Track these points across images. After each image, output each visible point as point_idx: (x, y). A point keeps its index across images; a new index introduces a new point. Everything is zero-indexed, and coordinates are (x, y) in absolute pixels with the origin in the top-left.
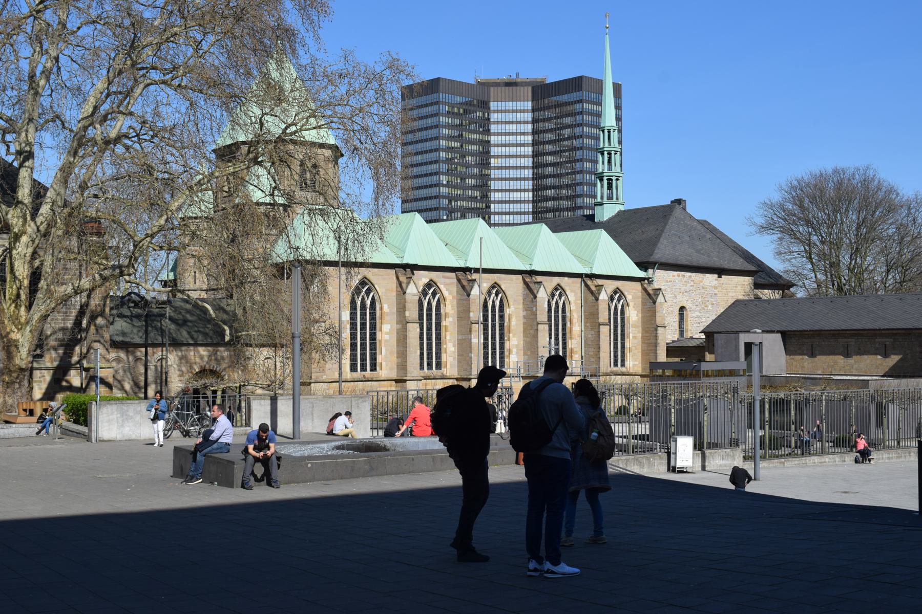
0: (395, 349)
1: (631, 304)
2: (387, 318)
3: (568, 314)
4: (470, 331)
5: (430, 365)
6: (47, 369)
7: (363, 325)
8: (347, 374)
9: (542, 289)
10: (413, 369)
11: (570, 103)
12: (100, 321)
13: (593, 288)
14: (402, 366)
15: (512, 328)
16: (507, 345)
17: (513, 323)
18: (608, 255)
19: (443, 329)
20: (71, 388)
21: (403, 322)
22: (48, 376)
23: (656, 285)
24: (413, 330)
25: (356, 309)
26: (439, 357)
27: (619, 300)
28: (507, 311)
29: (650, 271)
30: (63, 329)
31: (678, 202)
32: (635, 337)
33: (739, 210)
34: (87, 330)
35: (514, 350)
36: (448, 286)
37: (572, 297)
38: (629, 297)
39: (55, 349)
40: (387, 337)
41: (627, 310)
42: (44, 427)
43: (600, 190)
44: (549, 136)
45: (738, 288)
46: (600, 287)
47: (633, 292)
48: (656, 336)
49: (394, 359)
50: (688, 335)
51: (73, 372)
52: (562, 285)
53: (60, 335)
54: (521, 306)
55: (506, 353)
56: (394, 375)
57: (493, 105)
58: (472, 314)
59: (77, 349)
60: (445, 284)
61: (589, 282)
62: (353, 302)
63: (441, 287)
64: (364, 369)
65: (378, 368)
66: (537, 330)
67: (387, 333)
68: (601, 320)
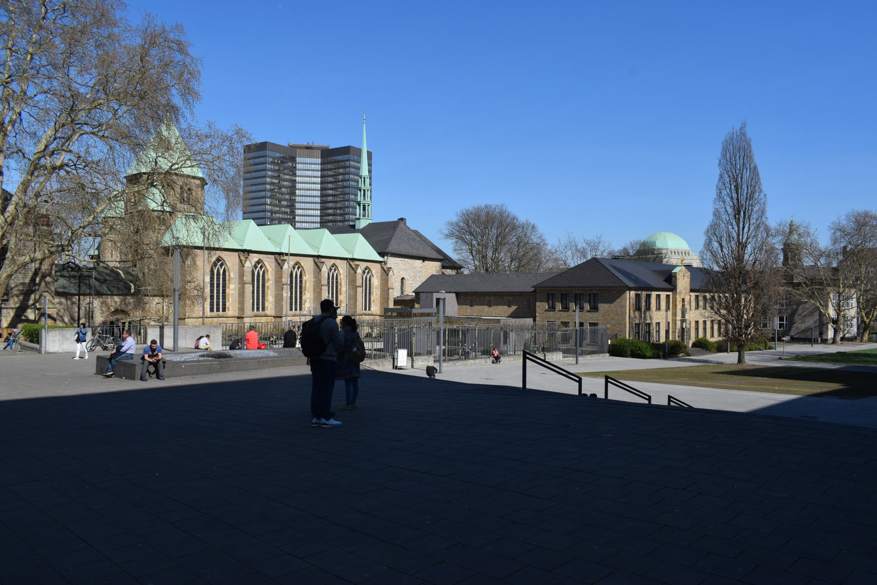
2: (233, 281)
5: (258, 309)
6: (12, 308)
12: (48, 279)
14: (242, 309)
16: (304, 297)
17: (308, 285)
20: (28, 320)
21: (242, 283)
22: (12, 313)
23: (388, 266)
24: (248, 288)
28: (304, 278)
30: (23, 284)
31: (402, 219)
33: (435, 224)
34: (39, 284)
36: (269, 263)
37: (341, 271)
38: (374, 272)
39: (17, 296)
40: (232, 292)
41: (372, 279)
42: (8, 345)
45: (434, 268)
47: (376, 269)
49: (237, 305)
51: (29, 311)
53: (21, 288)
56: (236, 314)
59: (32, 296)
60: (268, 262)
64: (218, 310)
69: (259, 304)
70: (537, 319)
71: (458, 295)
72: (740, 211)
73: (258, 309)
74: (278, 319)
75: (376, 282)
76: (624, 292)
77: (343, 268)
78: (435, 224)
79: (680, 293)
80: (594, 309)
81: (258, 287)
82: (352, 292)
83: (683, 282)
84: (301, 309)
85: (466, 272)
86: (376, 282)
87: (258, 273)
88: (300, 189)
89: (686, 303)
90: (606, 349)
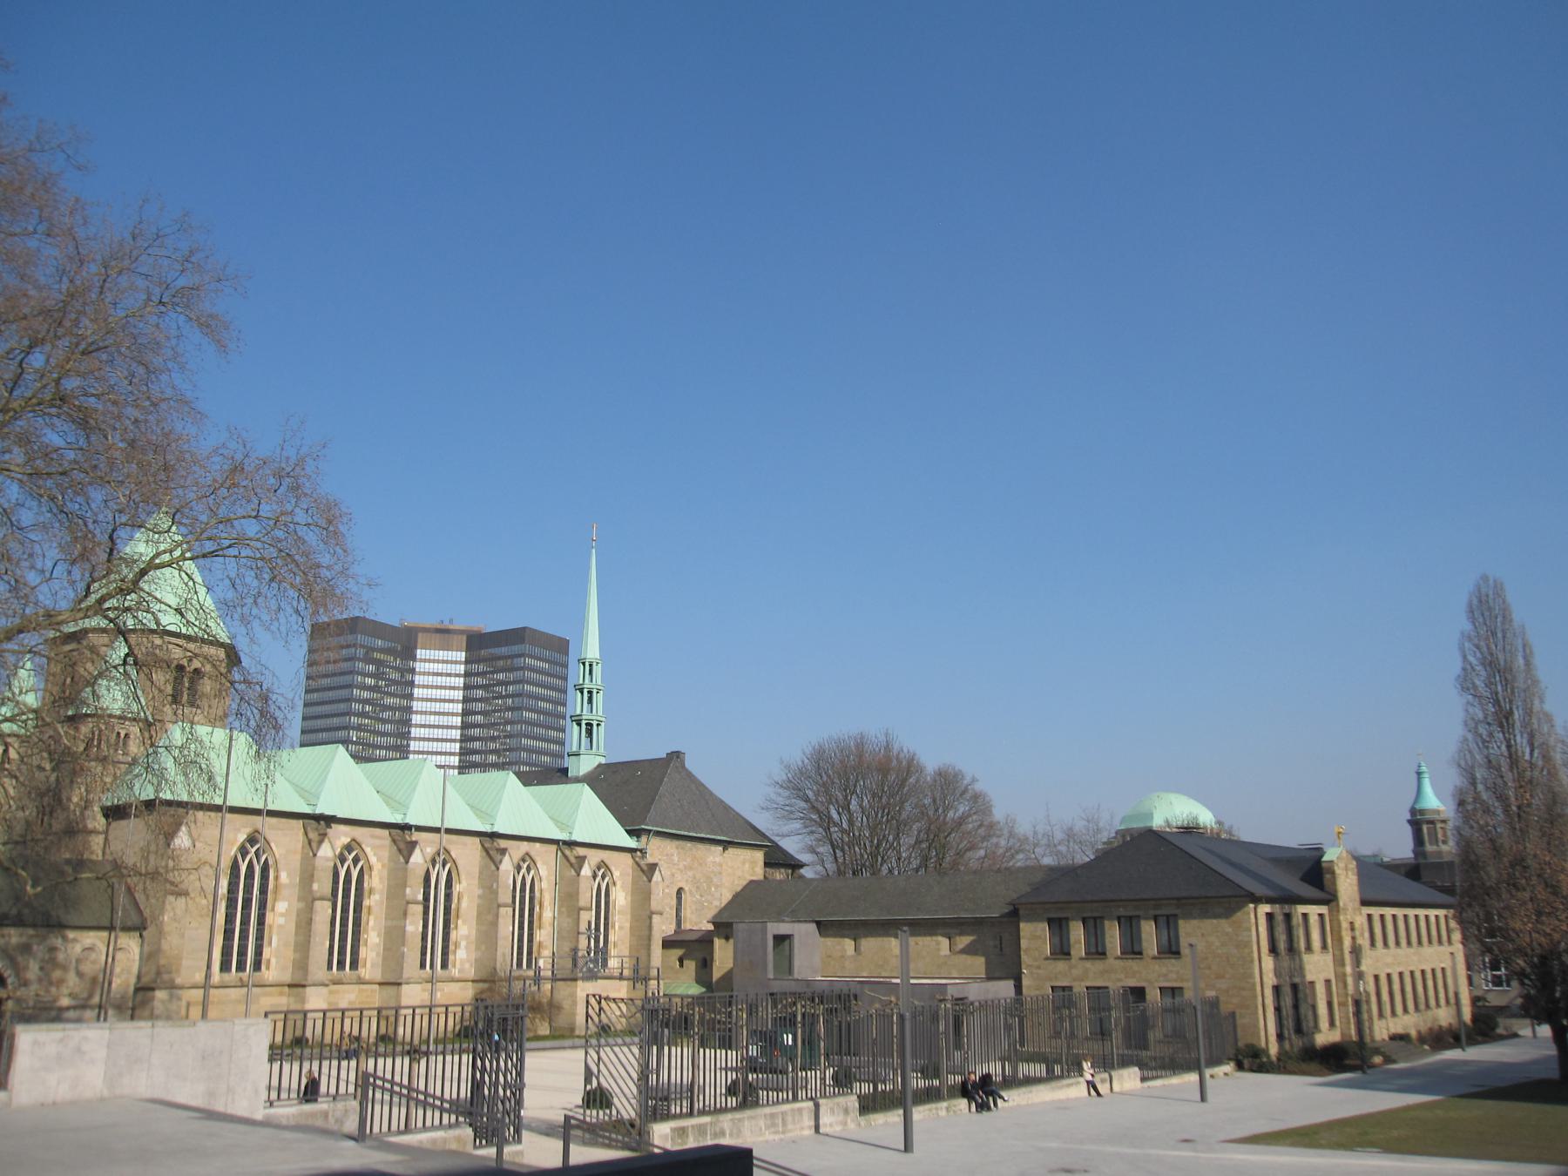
0: (292, 940)
1: (619, 883)
2: (284, 892)
3: (537, 894)
4: (405, 914)
5: (341, 964)
7: (247, 903)
8: (216, 975)
9: (507, 858)
10: (318, 969)
11: (512, 657)
13: (573, 860)
14: (302, 964)
15: (462, 911)
16: (453, 935)
17: (464, 904)
18: (595, 821)
19: (364, 911)
21: (308, 900)
23: (650, 859)
24: (323, 910)
25: (238, 877)
26: (355, 952)
27: (603, 877)
28: (457, 888)
29: (644, 838)
31: (676, 756)
32: (621, 928)
33: (747, 771)
35: (463, 944)
36: (377, 850)
37: (543, 871)
38: (616, 874)
40: (281, 921)
41: (613, 890)
43: (574, 733)
44: (480, 693)
45: (745, 866)
46: (582, 860)
47: (622, 867)
48: (650, 927)
49: (290, 954)
50: (686, 926)
52: (532, 854)
54: (476, 882)
55: (452, 947)
56: (287, 977)
57: (420, 653)
58: (408, 890)
60: (374, 847)
61: (567, 852)
62: (235, 867)
63: (368, 850)
64: (241, 967)
65: (263, 967)
66: (497, 916)
67: (282, 915)
68: (582, 903)
69: (345, 954)
70: (1025, 982)
71: (818, 923)
72: (1503, 719)
73: (341, 964)
74: (391, 990)
75: (621, 898)
76: (1244, 905)
77: (547, 865)
78: (747, 771)
79: (1345, 909)
80: (1171, 950)
81: (345, 910)
82: (567, 922)
83: (1347, 885)
84: (444, 965)
85: (807, 872)
86: (621, 898)
87: (348, 873)
88: (422, 713)
89: (1357, 933)
90: (1231, 1051)
